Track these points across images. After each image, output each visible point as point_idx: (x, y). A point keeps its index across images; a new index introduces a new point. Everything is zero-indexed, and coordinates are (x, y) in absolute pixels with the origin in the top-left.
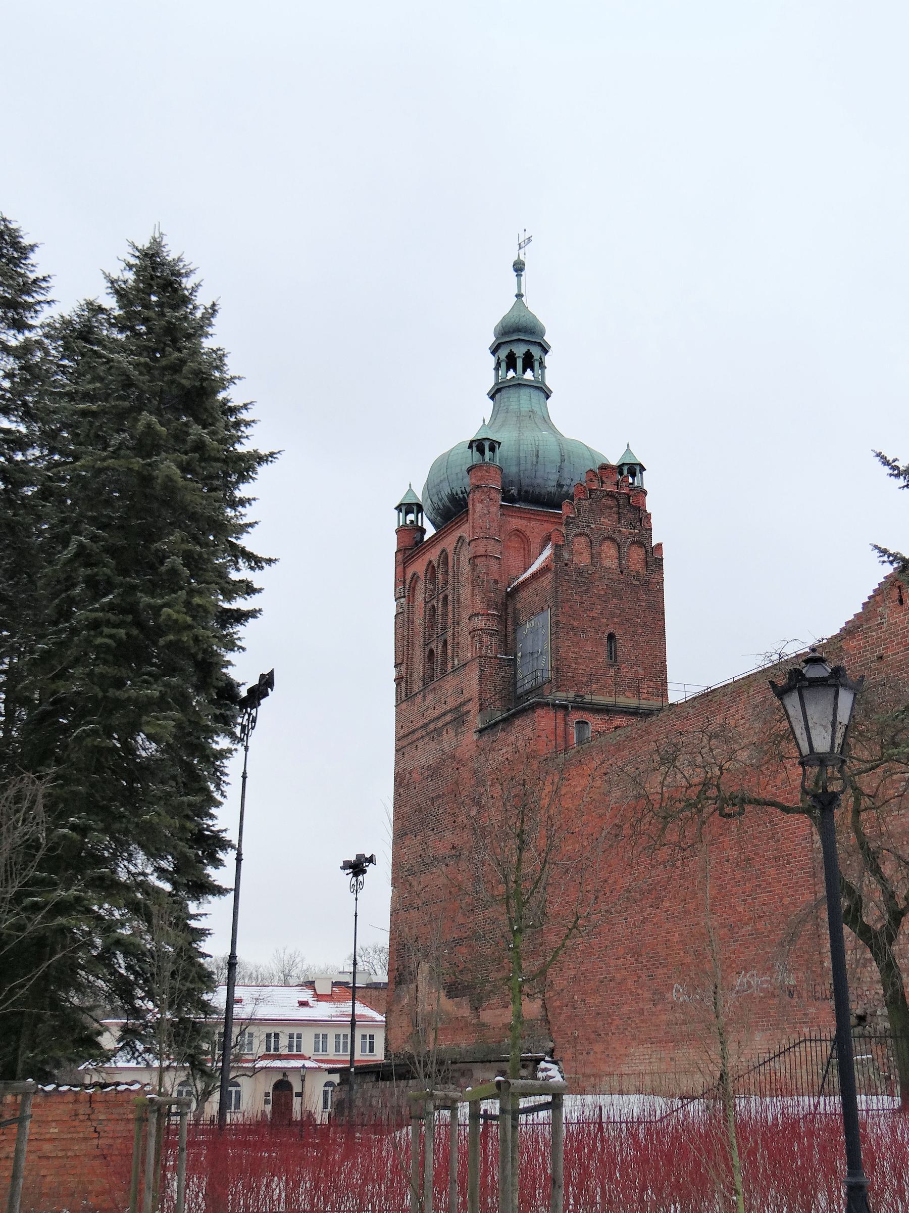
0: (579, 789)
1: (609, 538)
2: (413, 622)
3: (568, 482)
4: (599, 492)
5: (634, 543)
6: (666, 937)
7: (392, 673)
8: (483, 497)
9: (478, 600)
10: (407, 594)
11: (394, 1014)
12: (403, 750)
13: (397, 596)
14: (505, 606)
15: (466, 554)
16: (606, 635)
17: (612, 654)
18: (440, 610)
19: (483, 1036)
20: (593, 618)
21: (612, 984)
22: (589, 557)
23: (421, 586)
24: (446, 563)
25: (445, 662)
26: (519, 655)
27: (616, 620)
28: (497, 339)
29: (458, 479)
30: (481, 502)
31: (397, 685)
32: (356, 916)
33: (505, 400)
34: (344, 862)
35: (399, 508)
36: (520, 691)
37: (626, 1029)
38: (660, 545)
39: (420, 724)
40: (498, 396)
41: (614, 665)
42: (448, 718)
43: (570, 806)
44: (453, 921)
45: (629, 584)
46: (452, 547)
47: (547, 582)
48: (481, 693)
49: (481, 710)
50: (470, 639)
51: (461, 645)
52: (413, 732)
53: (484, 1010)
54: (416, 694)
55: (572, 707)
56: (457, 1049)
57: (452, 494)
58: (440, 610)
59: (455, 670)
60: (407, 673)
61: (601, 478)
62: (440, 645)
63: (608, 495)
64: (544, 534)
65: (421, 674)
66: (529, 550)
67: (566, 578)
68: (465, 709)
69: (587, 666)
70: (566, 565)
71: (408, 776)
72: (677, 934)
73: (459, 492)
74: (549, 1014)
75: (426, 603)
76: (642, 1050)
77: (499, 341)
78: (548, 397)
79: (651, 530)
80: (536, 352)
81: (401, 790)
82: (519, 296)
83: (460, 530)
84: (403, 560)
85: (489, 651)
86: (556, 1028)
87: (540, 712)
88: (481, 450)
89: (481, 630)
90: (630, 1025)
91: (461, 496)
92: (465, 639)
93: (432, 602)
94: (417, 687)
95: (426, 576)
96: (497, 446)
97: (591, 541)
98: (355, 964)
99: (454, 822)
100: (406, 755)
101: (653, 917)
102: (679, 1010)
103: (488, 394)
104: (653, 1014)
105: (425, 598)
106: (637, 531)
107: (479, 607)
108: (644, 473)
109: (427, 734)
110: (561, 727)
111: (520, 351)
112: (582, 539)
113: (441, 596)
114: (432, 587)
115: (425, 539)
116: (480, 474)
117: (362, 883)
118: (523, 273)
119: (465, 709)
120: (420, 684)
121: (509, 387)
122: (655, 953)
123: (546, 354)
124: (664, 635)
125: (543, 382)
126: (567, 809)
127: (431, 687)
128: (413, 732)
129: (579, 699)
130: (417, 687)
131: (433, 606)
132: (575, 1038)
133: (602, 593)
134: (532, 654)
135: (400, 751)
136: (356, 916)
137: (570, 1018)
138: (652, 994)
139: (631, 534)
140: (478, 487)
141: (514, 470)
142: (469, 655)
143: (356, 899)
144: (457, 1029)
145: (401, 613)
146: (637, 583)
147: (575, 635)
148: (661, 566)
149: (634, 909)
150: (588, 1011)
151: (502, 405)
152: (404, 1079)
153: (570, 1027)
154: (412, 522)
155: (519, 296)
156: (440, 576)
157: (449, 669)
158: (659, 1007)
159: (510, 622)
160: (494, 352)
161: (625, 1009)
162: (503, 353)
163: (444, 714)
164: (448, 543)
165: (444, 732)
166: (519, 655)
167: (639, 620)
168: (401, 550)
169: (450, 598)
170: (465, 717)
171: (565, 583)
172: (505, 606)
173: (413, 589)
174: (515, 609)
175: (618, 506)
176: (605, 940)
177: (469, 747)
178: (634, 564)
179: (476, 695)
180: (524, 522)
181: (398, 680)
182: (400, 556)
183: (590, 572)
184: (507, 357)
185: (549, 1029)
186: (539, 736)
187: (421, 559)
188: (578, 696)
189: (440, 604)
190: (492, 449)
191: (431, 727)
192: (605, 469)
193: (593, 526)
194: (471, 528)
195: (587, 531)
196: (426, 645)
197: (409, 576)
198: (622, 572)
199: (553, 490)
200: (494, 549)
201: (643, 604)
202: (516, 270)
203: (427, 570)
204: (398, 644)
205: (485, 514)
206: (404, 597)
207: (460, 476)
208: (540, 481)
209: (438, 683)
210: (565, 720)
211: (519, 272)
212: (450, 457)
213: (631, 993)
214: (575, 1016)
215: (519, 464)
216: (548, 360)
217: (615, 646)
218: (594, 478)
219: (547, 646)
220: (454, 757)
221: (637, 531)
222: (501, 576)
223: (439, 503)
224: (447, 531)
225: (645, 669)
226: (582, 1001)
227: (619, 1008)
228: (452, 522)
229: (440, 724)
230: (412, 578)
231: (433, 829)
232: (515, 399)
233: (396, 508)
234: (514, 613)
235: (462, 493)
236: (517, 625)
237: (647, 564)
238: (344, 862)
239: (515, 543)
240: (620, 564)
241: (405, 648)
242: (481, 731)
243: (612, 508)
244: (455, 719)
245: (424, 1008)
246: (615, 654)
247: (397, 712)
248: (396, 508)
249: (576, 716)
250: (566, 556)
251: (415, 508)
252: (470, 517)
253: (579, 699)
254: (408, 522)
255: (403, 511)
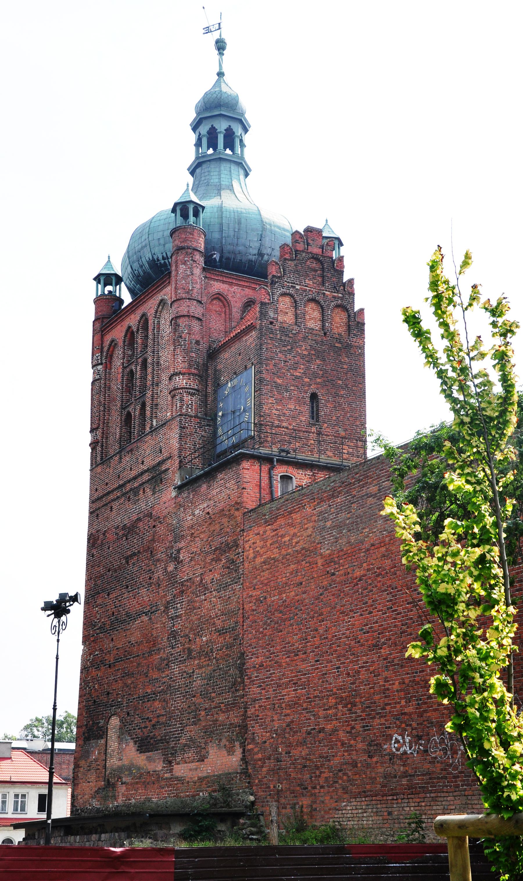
0: (287, 539)
1: (313, 300)
2: (109, 388)
3: (269, 251)
4: (304, 254)
5: (337, 306)
6: (384, 686)
7: (88, 438)
8: (186, 259)
9: (180, 359)
10: (104, 361)
11: (81, 770)
12: (98, 512)
13: (94, 363)
14: (206, 367)
15: (167, 316)
16: (309, 395)
17: (315, 415)
18: (138, 373)
19: (176, 790)
20: (297, 377)
21: (321, 735)
22: (292, 317)
23: (119, 352)
24: (145, 327)
25: (143, 426)
26: (220, 414)
27: (318, 380)
28: (198, 114)
29: (160, 244)
30: (185, 263)
31: (92, 449)
32: (57, 659)
33: (206, 174)
34: (46, 603)
35: (97, 279)
36: (219, 449)
37: (337, 782)
38: (362, 311)
39: (116, 485)
40: (198, 171)
41: (316, 425)
42: (146, 477)
43: (277, 556)
44: (147, 676)
45: (332, 346)
46: (153, 311)
47: (251, 340)
48: (180, 449)
49: (180, 467)
50: (169, 398)
51: (159, 407)
52: (108, 493)
53: (178, 764)
54: (111, 457)
55: (278, 461)
56: (147, 804)
57: (153, 260)
58: (138, 373)
59: (153, 430)
60: (103, 437)
61: (307, 241)
62: (138, 408)
63: (313, 258)
64: (245, 300)
65: (118, 437)
66: (230, 314)
67: (271, 336)
68: (163, 468)
69: (290, 424)
70: (271, 323)
71: (101, 536)
72: (397, 682)
73: (160, 258)
74: (249, 767)
75: (124, 368)
76: (355, 803)
77: (201, 116)
78: (247, 175)
79: (354, 295)
80: (238, 130)
81: (94, 552)
82: (220, 74)
83: (161, 293)
84: (101, 329)
85: (190, 410)
86: (257, 781)
87: (246, 464)
88: (185, 216)
89: (182, 388)
90: (341, 778)
91: (162, 262)
92: (165, 398)
93: (130, 366)
94: (114, 448)
95: (124, 342)
96: (201, 210)
97: (295, 302)
98: (55, 709)
99: (150, 578)
100: (100, 517)
101: (370, 666)
102: (398, 762)
103: (188, 169)
104: (368, 766)
105: (123, 363)
106: (340, 295)
107: (181, 364)
108: (341, 248)
109: (123, 495)
110: (265, 482)
111: (222, 126)
112: (287, 299)
113: (140, 360)
114: (130, 353)
115: (123, 307)
116: (183, 236)
117: (65, 624)
118: (224, 52)
119: (163, 468)
120: (117, 447)
121: (209, 161)
122: (371, 703)
123: (246, 133)
124: (364, 398)
125: (242, 158)
126: (274, 559)
127: (128, 449)
128: (108, 493)
129: (284, 454)
130: (114, 448)
131: (132, 371)
132: (278, 791)
133: (305, 353)
134: (234, 412)
135: (94, 513)
136: (57, 659)
137: (273, 771)
138: (367, 745)
139: (334, 297)
140: (182, 248)
141: (216, 235)
142: (168, 414)
143: (58, 641)
144: (148, 784)
145: (98, 379)
146: (340, 345)
147: (279, 393)
148: (362, 331)
149: (348, 658)
150: (294, 764)
151: (203, 179)
152: (96, 833)
153: (272, 780)
154: (110, 292)
155: (220, 74)
156: (139, 341)
157: (148, 429)
158: (375, 759)
159: (210, 383)
160: (194, 129)
161: (336, 761)
162: (204, 129)
163: (142, 474)
164: (149, 308)
165: (141, 492)
166: (220, 414)
167: (340, 382)
168: (100, 318)
169: (149, 360)
170: (163, 475)
171: (269, 341)
172: (206, 367)
173: (110, 357)
174: (216, 370)
175: (323, 269)
176: (315, 690)
177: (166, 505)
178: (337, 327)
179: (176, 453)
180: (225, 286)
181: (94, 445)
182: (98, 325)
183: (294, 332)
184: (208, 133)
185: (249, 783)
186: (243, 488)
187: (120, 326)
188: (283, 451)
189: (139, 368)
190: (196, 214)
191: (128, 487)
192: (311, 232)
193: (298, 287)
194: (173, 289)
195: (292, 291)
196: (123, 408)
197: (107, 343)
198: (325, 334)
199: (253, 258)
200: (197, 310)
201: (345, 366)
202: (219, 49)
203: (125, 336)
204: (95, 410)
205: (189, 276)
206: (101, 364)
207: (162, 241)
208: (241, 248)
209: (135, 445)
210: (270, 473)
211: (221, 51)
212: (152, 224)
213: (343, 744)
214: (279, 769)
215: (221, 231)
216: (247, 139)
217: (317, 406)
218: (300, 240)
219: (251, 403)
220: (150, 515)
221: (340, 295)
222: (203, 338)
223: (140, 270)
224: (147, 295)
225: (346, 430)
226: (286, 753)
227: (329, 760)
228: (153, 286)
229: (136, 485)
230: (110, 345)
231: (127, 587)
232: (216, 173)
233: (95, 279)
234: (215, 374)
235: (164, 258)
236: (218, 386)
237: (349, 327)
238: (46, 603)
239: (216, 306)
240: (323, 326)
241: (102, 413)
242: (180, 488)
243: (316, 271)
244: (153, 478)
245: (113, 762)
246: (317, 414)
247: (91, 476)
248: (95, 279)
249: (280, 471)
250: (271, 314)
251: (114, 278)
252: (173, 279)
253: (284, 454)
254: (106, 292)
255: (102, 281)
